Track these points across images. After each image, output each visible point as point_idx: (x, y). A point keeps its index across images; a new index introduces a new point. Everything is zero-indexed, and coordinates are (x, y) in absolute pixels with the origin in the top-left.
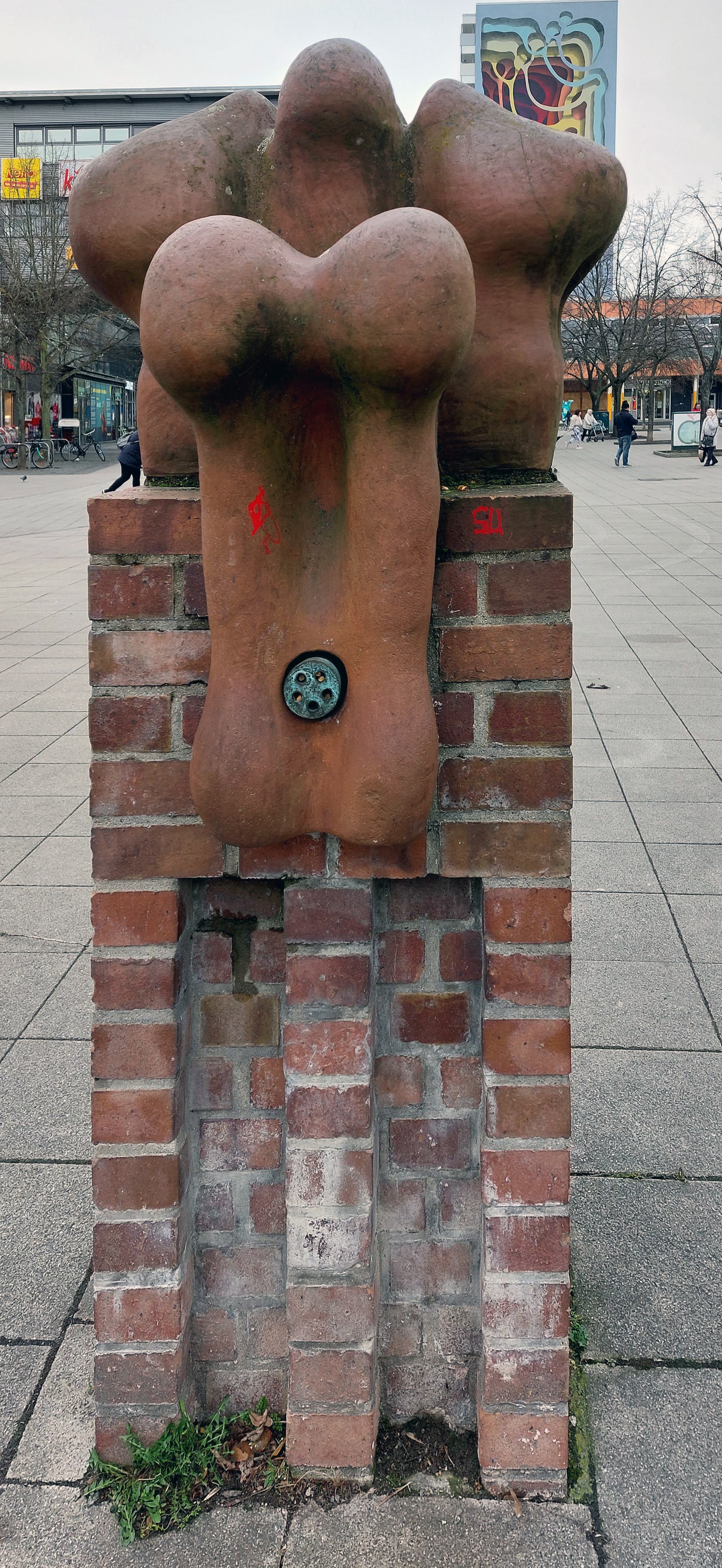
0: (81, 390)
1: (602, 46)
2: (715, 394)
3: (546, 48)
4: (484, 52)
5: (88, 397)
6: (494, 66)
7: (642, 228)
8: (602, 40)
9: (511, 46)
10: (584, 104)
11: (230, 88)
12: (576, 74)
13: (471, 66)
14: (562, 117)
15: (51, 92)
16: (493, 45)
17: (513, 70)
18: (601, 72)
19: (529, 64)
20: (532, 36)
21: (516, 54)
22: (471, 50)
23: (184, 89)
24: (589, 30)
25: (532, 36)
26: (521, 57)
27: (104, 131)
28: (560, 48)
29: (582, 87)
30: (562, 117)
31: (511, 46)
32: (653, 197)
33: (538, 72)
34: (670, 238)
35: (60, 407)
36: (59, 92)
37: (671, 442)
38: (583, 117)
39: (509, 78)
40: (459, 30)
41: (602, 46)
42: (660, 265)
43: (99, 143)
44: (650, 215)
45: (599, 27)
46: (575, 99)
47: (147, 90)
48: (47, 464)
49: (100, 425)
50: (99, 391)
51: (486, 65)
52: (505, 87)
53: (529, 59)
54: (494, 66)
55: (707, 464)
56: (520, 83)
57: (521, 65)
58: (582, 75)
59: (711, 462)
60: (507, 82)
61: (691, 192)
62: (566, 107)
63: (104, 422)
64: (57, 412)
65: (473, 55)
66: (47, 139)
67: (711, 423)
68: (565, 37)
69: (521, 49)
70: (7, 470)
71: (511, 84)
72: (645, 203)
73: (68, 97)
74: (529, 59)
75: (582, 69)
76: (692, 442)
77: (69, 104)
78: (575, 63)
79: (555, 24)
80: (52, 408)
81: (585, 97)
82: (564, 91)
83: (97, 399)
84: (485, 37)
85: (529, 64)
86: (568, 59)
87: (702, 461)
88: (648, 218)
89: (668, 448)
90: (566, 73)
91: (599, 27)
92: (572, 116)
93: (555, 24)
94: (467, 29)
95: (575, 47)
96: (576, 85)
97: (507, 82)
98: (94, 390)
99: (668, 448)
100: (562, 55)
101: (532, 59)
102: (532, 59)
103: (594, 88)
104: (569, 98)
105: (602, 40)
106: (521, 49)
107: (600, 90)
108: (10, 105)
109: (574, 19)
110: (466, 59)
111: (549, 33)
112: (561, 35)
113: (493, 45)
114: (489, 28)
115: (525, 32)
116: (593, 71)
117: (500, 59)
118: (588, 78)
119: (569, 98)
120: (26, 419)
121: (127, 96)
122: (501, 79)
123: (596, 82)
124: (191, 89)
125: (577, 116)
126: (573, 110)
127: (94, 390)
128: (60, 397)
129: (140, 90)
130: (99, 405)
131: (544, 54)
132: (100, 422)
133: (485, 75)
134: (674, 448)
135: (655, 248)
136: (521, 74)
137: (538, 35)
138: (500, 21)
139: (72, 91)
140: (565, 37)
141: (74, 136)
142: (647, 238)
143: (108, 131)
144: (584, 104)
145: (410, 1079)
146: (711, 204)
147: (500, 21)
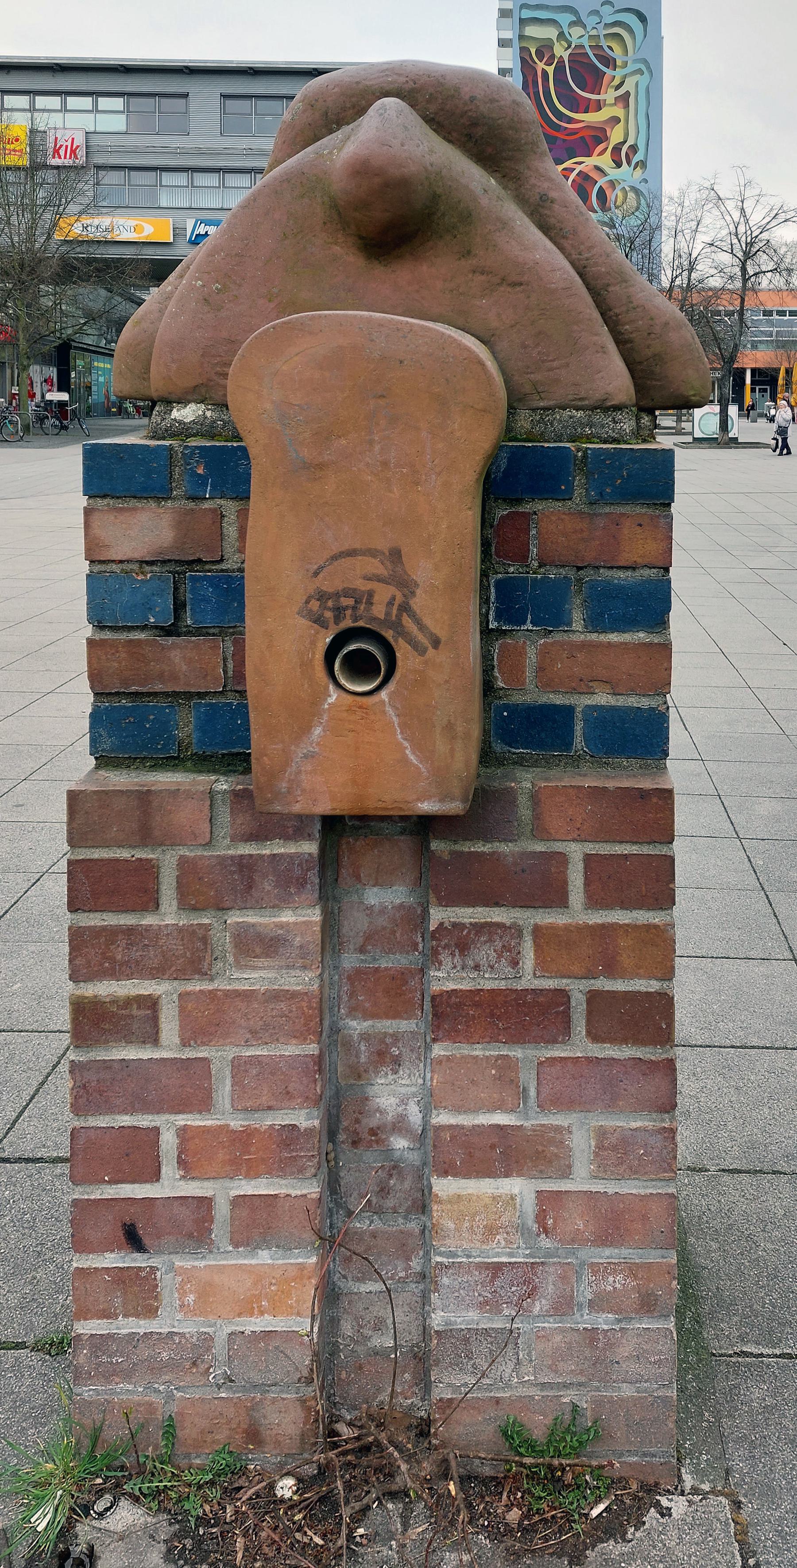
0: (80, 363)
1: (645, 36)
2: (768, 387)
3: (587, 36)
4: (522, 37)
5: (89, 369)
6: (533, 51)
7: (673, 218)
8: (645, 30)
9: (551, 33)
10: (628, 94)
11: (334, 64)
12: (619, 63)
13: (509, 51)
14: (605, 105)
15: (39, 58)
16: (531, 31)
17: (553, 56)
18: (645, 62)
19: (570, 51)
20: (572, 24)
21: (555, 41)
22: (508, 35)
23: (184, 61)
24: (632, 20)
25: (572, 24)
26: (561, 44)
27: (65, 99)
28: (602, 37)
29: (625, 76)
30: (605, 105)
31: (551, 33)
32: (685, 188)
33: (578, 59)
34: (704, 229)
35: (55, 380)
36: (47, 58)
37: (692, 433)
38: (627, 106)
39: (549, 64)
40: (496, 15)
41: (645, 36)
42: (694, 256)
43: (61, 111)
44: (682, 204)
45: (642, 18)
46: (618, 88)
47: (143, 60)
48: (18, 438)
49: (102, 399)
50: (101, 365)
51: (523, 49)
52: (545, 74)
53: (569, 46)
54: (533, 51)
55: (781, 454)
56: (560, 69)
57: (560, 51)
58: (625, 64)
59: (785, 451)
60: (546, 68)
61: (707, 184)
62: (609, 95)
63: (107, 397)
64: (52, 385)
65: (511, 40)
66: (66, 106)
67: (785, 416)
68: (607, 25)
69: (561, 36)
70: (6, 443)
71: (550, 70)
72: (676, 194)
73: (57, 64)
74: (569, 46)
75: (625, 59)
76: (714, 433)
77: (58, 71)
78: (617, 53)
79: (596, 12)
80: (46, 381)
81: (629, 86)
82: (606, 80)
83: (100, 373)
84: (523, 22)
85: (570, 51)
86: (610, 48)
87: (774, 451)
88: (680, 209)
89: (689, 439)
90: (609, 62)
91: (642, 18)
92: (615, 104)
93: (596, 12)
94: (504, 13)
95: (617, 36)
96: (619, 73)
97: (546, 68)
98: (96, 364)
99: (689, 439)
100: (604, 43)
101: (573, 46)
102: (573, 46)
103: (637, 77)
104: (612, 87)
105: (645, 30)
106: (561, 36)
107: (644, 80)
108: (124, 72)
109: (616, 9)
110: (503, 43)
111: (591, 21)
112: (602, 24)
113: (531, 31)
114: (527, 14)
115: (564, 19)
116: (636, 61)
117: (538, 45)
118: (631, 67)
119: (612, 87)
120: (13, 392)
121: (122, 66)
122: (540, 65)
123: (640, 72)
124: (191, 61)
125: (621, 105)
126: (616, 99)
127: (96, 364)
128: (55, 370)
129: (135, 60)
130: (101, 379)
131: (585, 42)
132: (103, 397)
133: (522, 59)
134: (694, 439)
135: (688, 239)
136: (561, 60)
137: (578, 22)
138: (538, 7)
139: (61, 58)
140: (607, 25)
141: (96, 104)
142: (679, 228)
143: (70, 100)
144: (628, 94)
145: (509, 1053)
146: (727, 196)
147: (538, 7)
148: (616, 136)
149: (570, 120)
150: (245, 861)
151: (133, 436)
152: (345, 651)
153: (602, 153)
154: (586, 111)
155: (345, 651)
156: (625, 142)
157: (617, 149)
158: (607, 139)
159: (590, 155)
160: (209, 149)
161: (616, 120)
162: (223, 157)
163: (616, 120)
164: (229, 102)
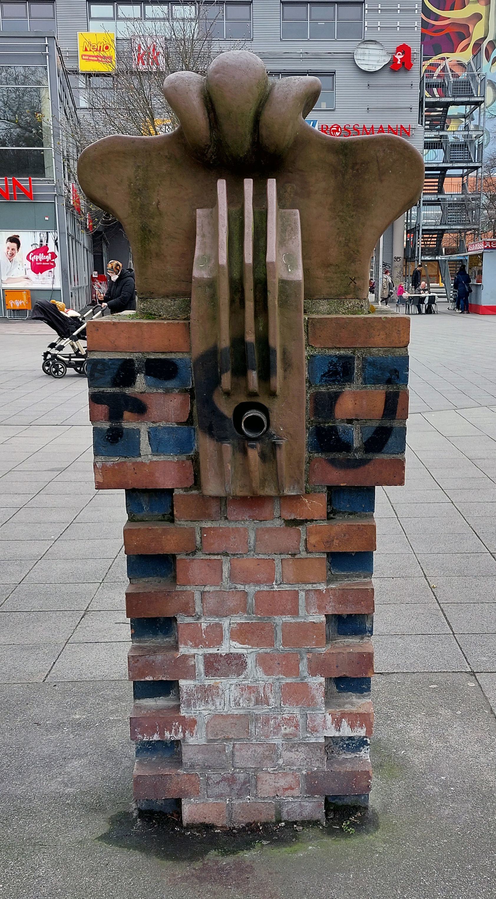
43: (112, 19)
148: (477, 33)
149: (438, 18)
150: (106, 165)
151: (259, 459)
152: (243, 420)
153: (464, 49)
154: (452, 9)
155: (243, 420)
156: (485, 38)
157: (478, 45)
158: (469, 35)
159: (454, 51)
160: (270, 53)
161: (478, 17)
162: (285, 61)
163: (478, 17)
164: (287, 8)
